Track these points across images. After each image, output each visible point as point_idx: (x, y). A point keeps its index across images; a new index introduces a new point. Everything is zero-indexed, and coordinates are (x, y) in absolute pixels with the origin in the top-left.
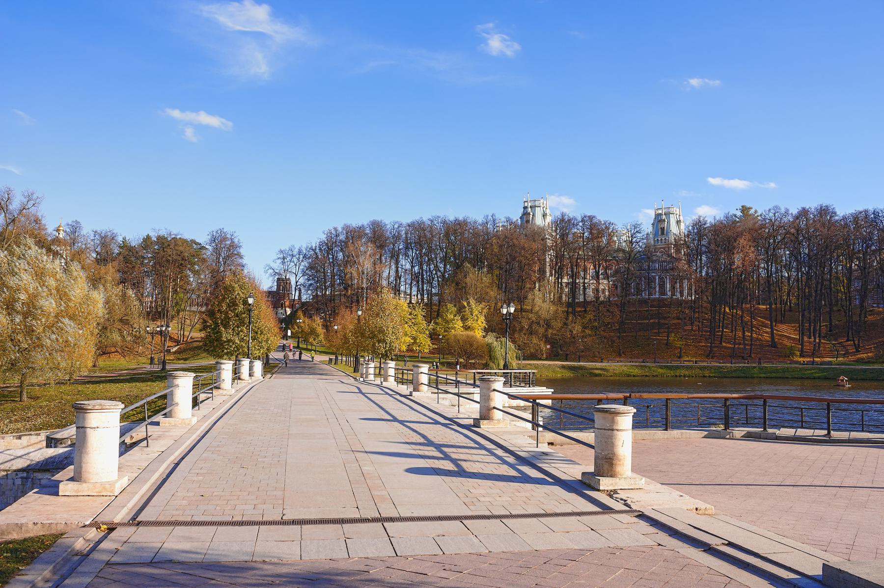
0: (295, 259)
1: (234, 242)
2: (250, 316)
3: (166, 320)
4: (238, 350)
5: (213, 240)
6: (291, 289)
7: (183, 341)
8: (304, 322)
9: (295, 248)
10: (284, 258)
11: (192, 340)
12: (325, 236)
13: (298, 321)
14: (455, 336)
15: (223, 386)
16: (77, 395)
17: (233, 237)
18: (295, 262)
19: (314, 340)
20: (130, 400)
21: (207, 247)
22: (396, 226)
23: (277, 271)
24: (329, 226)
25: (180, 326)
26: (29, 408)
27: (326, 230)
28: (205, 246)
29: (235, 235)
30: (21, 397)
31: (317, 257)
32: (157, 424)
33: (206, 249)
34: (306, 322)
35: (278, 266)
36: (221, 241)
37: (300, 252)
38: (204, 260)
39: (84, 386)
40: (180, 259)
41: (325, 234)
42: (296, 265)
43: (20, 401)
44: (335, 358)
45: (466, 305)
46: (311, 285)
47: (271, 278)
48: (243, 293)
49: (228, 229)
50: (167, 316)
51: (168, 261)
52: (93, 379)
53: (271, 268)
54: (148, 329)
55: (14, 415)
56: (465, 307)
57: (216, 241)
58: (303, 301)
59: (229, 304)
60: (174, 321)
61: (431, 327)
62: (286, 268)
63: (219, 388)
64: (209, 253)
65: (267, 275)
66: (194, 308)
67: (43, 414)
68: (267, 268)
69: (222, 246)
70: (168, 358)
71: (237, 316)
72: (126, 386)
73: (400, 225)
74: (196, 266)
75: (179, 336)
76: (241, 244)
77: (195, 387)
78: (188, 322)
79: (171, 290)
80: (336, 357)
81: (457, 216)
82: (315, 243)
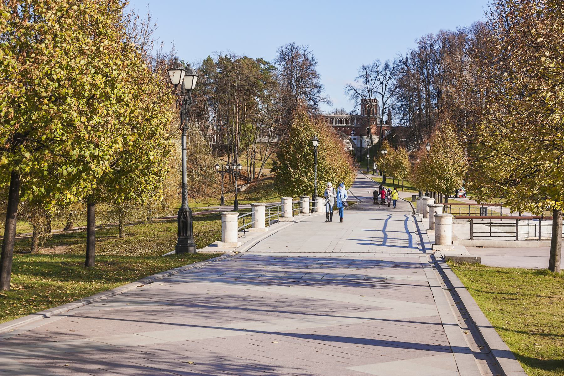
0: (381, 77)
1: (307, 59)
2: (315, 157)
3: (233, 154)
4: (307, 188)
5: (283, 57)
6: (378, 112)
7: (254, 178)
8: (389, 153)
10: (367, 76)
11: (264, 177)
12: (418, 45)
13: (383, 152)
15: (286, 215)
16: (166, 231)
17: (306, 53)
18: (381, 80)
19: (400, 174)
20: (213, 234)
21: (277, 66)
23: (360, 92)
24: (422, 34)
25: (249, 162)
26: (129, 242)
27: (419, 39)
28: (273, 65)
29: (309, 50)
30: (120, 234)
31: (408, 72)
32: (248, 232)
33: (276, 69)
34: (392, 153)
35: (360, 85)
36: (292, 60)
37: (387, 68)
38: (273, 84)
39: (170, 224)
40: (246, 84)
41: (417, 43)
42: (382, 83)
43: (120, 237)
44: (418, 194)
46: (402, 106)
47: (353, 101)
48: (308, 135)
49: (300, 43)
50: (235, 150)
51: (233, 87)
53: (352, 88)
54: (217, 167)
55: (119, 247)
57: (287, 58)
58: (393, 126)
59: (295, 146)
60: (243, 156)
62: (371, 87)
63: (284, 217)
64: (278, 73)
65: (349, 97)
66: (265, 140)
67: (142, 247)
69: (294, 64)
70: (239, 198)
71: (304, 157)
72: (208, 223)
74: (265, 91)
75: (249, 173)
76: (316, 61)
77: (267, 222)
78: (258, 156)
79: (237, 120)
80: (419, 193)
82: (405, 54)
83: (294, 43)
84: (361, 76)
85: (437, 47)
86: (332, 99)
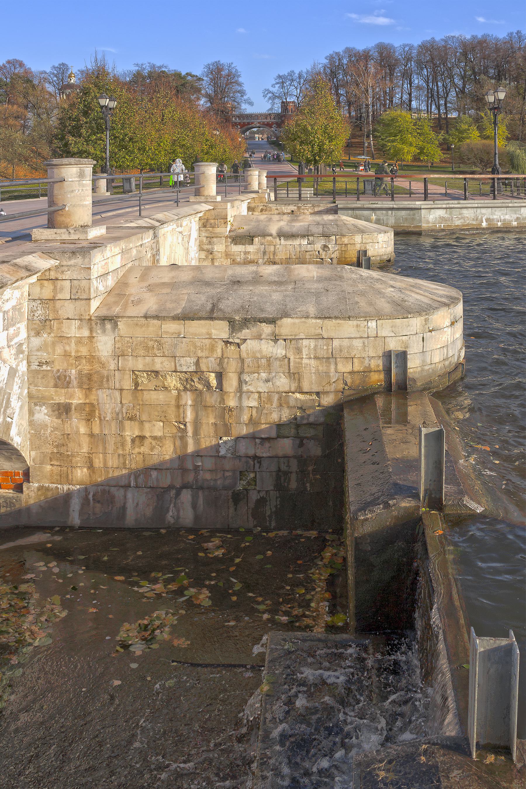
0: (295, 83)
9: (295, 73)
14: (468, 145)
18: (296, 86)
22: (407, 49)
23: (277, 95)
24: (329, 52)
37: (300, 76)
45: (483, 116)
49: (224, 61)
52: (16, 194)
53: (270, 92)
56: (482, 118)
61: (440, 137)
65: (267, 99)
68: (266, 92)
72: (395, 206)
73: (411, 47)
76: (239, 73)
81: (475, 34)
83: (219, 61)
84: (277, 83)
85: (345, 61)
86: (253, 100)
